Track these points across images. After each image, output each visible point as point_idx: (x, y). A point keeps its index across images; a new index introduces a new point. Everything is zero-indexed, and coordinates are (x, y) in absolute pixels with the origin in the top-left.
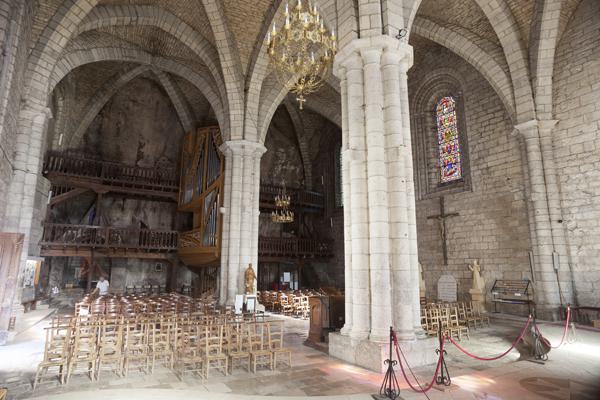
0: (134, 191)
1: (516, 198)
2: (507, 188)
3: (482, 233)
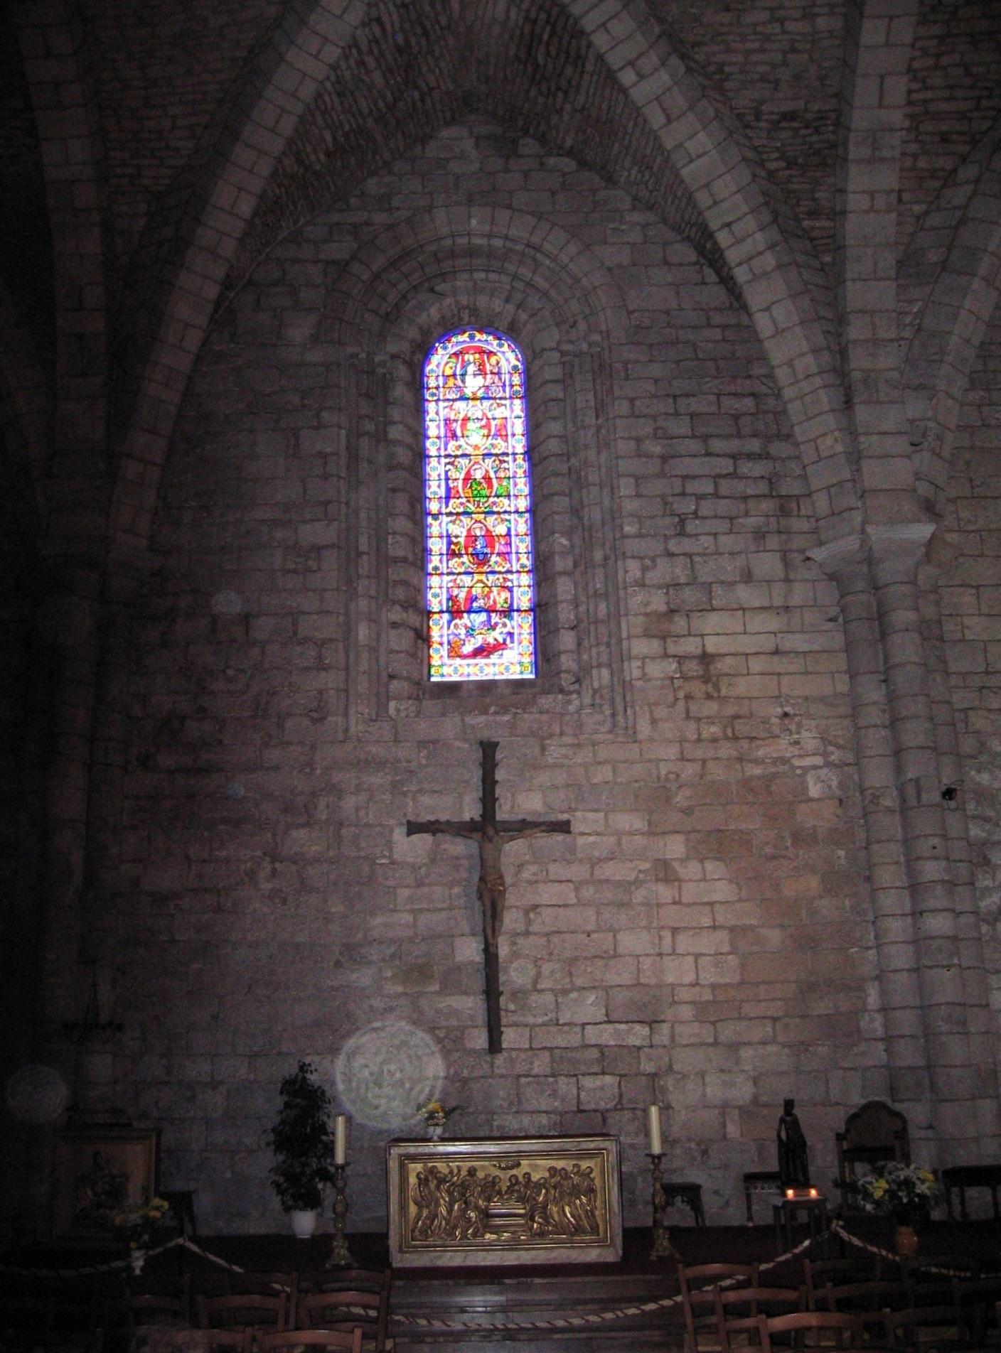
1: (814, 790)
2: (782, 747)
3: (670, 916)
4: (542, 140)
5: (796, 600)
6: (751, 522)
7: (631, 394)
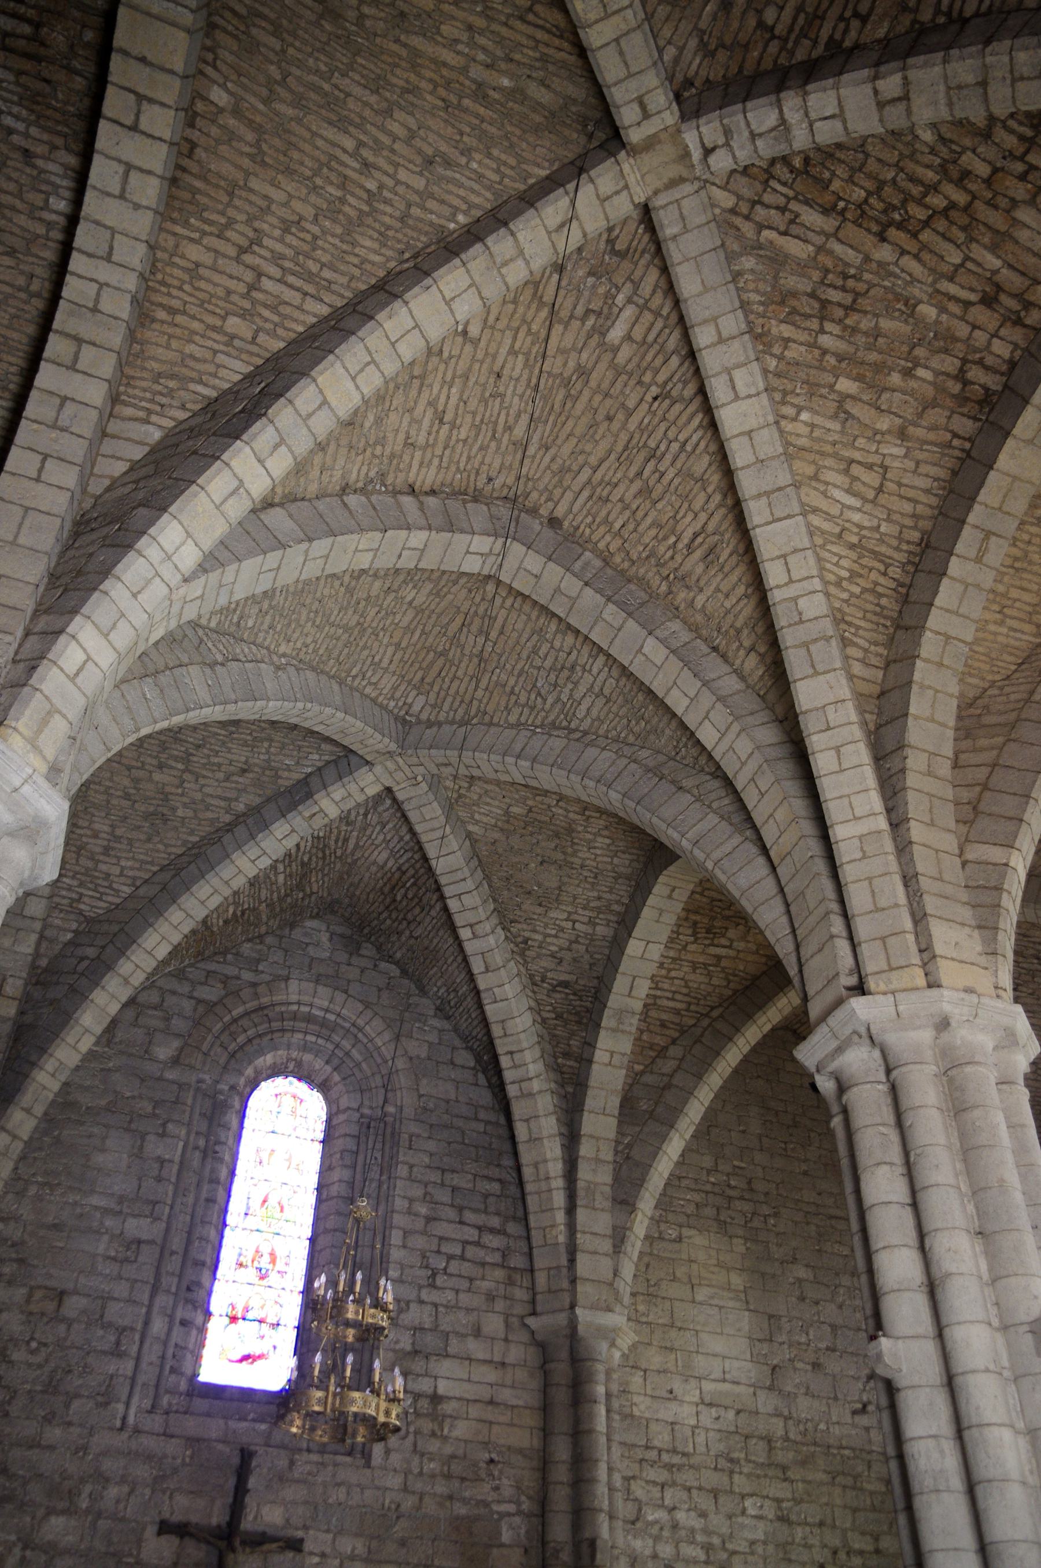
0: (358, 1177)
1: (506, 1536)
2: (484, 1491)
4: (379, 949)
5: (511, 1359)
6: (486, 1285)
7: (412, 1161)
